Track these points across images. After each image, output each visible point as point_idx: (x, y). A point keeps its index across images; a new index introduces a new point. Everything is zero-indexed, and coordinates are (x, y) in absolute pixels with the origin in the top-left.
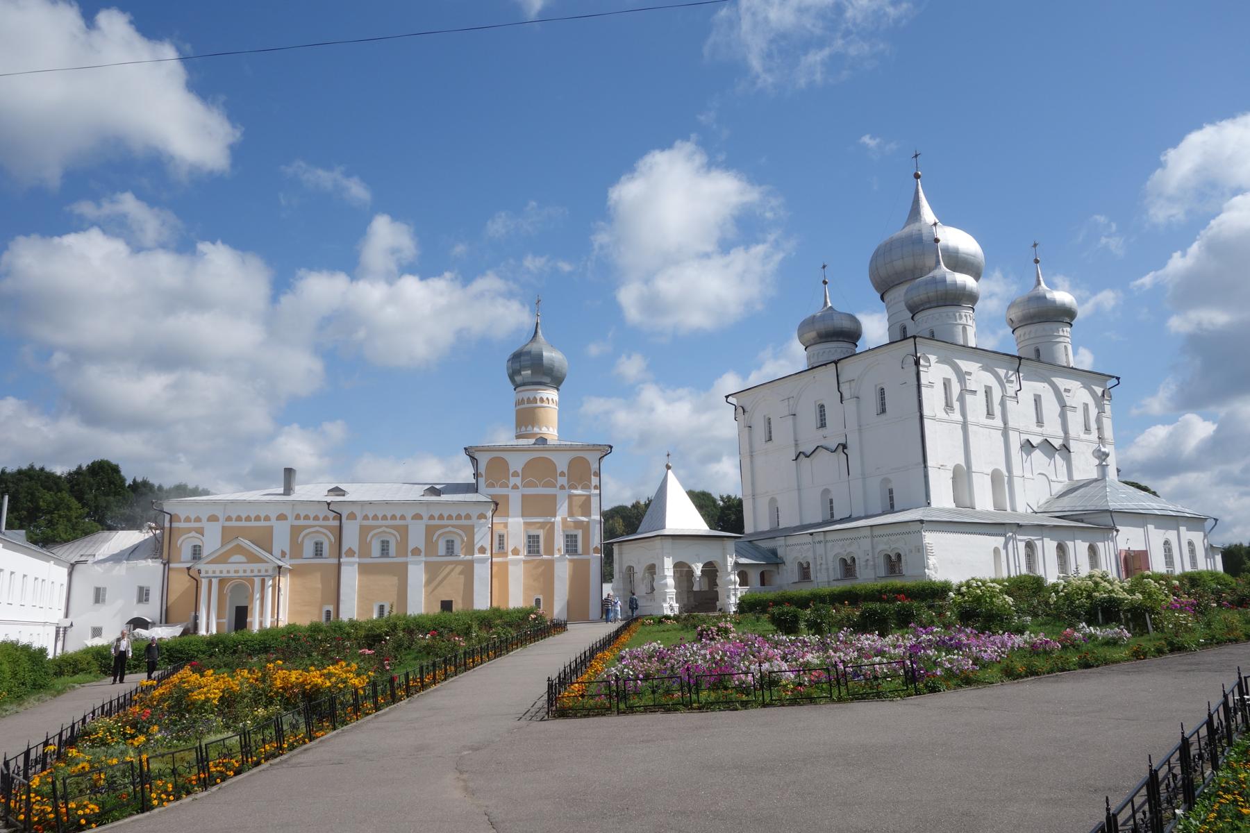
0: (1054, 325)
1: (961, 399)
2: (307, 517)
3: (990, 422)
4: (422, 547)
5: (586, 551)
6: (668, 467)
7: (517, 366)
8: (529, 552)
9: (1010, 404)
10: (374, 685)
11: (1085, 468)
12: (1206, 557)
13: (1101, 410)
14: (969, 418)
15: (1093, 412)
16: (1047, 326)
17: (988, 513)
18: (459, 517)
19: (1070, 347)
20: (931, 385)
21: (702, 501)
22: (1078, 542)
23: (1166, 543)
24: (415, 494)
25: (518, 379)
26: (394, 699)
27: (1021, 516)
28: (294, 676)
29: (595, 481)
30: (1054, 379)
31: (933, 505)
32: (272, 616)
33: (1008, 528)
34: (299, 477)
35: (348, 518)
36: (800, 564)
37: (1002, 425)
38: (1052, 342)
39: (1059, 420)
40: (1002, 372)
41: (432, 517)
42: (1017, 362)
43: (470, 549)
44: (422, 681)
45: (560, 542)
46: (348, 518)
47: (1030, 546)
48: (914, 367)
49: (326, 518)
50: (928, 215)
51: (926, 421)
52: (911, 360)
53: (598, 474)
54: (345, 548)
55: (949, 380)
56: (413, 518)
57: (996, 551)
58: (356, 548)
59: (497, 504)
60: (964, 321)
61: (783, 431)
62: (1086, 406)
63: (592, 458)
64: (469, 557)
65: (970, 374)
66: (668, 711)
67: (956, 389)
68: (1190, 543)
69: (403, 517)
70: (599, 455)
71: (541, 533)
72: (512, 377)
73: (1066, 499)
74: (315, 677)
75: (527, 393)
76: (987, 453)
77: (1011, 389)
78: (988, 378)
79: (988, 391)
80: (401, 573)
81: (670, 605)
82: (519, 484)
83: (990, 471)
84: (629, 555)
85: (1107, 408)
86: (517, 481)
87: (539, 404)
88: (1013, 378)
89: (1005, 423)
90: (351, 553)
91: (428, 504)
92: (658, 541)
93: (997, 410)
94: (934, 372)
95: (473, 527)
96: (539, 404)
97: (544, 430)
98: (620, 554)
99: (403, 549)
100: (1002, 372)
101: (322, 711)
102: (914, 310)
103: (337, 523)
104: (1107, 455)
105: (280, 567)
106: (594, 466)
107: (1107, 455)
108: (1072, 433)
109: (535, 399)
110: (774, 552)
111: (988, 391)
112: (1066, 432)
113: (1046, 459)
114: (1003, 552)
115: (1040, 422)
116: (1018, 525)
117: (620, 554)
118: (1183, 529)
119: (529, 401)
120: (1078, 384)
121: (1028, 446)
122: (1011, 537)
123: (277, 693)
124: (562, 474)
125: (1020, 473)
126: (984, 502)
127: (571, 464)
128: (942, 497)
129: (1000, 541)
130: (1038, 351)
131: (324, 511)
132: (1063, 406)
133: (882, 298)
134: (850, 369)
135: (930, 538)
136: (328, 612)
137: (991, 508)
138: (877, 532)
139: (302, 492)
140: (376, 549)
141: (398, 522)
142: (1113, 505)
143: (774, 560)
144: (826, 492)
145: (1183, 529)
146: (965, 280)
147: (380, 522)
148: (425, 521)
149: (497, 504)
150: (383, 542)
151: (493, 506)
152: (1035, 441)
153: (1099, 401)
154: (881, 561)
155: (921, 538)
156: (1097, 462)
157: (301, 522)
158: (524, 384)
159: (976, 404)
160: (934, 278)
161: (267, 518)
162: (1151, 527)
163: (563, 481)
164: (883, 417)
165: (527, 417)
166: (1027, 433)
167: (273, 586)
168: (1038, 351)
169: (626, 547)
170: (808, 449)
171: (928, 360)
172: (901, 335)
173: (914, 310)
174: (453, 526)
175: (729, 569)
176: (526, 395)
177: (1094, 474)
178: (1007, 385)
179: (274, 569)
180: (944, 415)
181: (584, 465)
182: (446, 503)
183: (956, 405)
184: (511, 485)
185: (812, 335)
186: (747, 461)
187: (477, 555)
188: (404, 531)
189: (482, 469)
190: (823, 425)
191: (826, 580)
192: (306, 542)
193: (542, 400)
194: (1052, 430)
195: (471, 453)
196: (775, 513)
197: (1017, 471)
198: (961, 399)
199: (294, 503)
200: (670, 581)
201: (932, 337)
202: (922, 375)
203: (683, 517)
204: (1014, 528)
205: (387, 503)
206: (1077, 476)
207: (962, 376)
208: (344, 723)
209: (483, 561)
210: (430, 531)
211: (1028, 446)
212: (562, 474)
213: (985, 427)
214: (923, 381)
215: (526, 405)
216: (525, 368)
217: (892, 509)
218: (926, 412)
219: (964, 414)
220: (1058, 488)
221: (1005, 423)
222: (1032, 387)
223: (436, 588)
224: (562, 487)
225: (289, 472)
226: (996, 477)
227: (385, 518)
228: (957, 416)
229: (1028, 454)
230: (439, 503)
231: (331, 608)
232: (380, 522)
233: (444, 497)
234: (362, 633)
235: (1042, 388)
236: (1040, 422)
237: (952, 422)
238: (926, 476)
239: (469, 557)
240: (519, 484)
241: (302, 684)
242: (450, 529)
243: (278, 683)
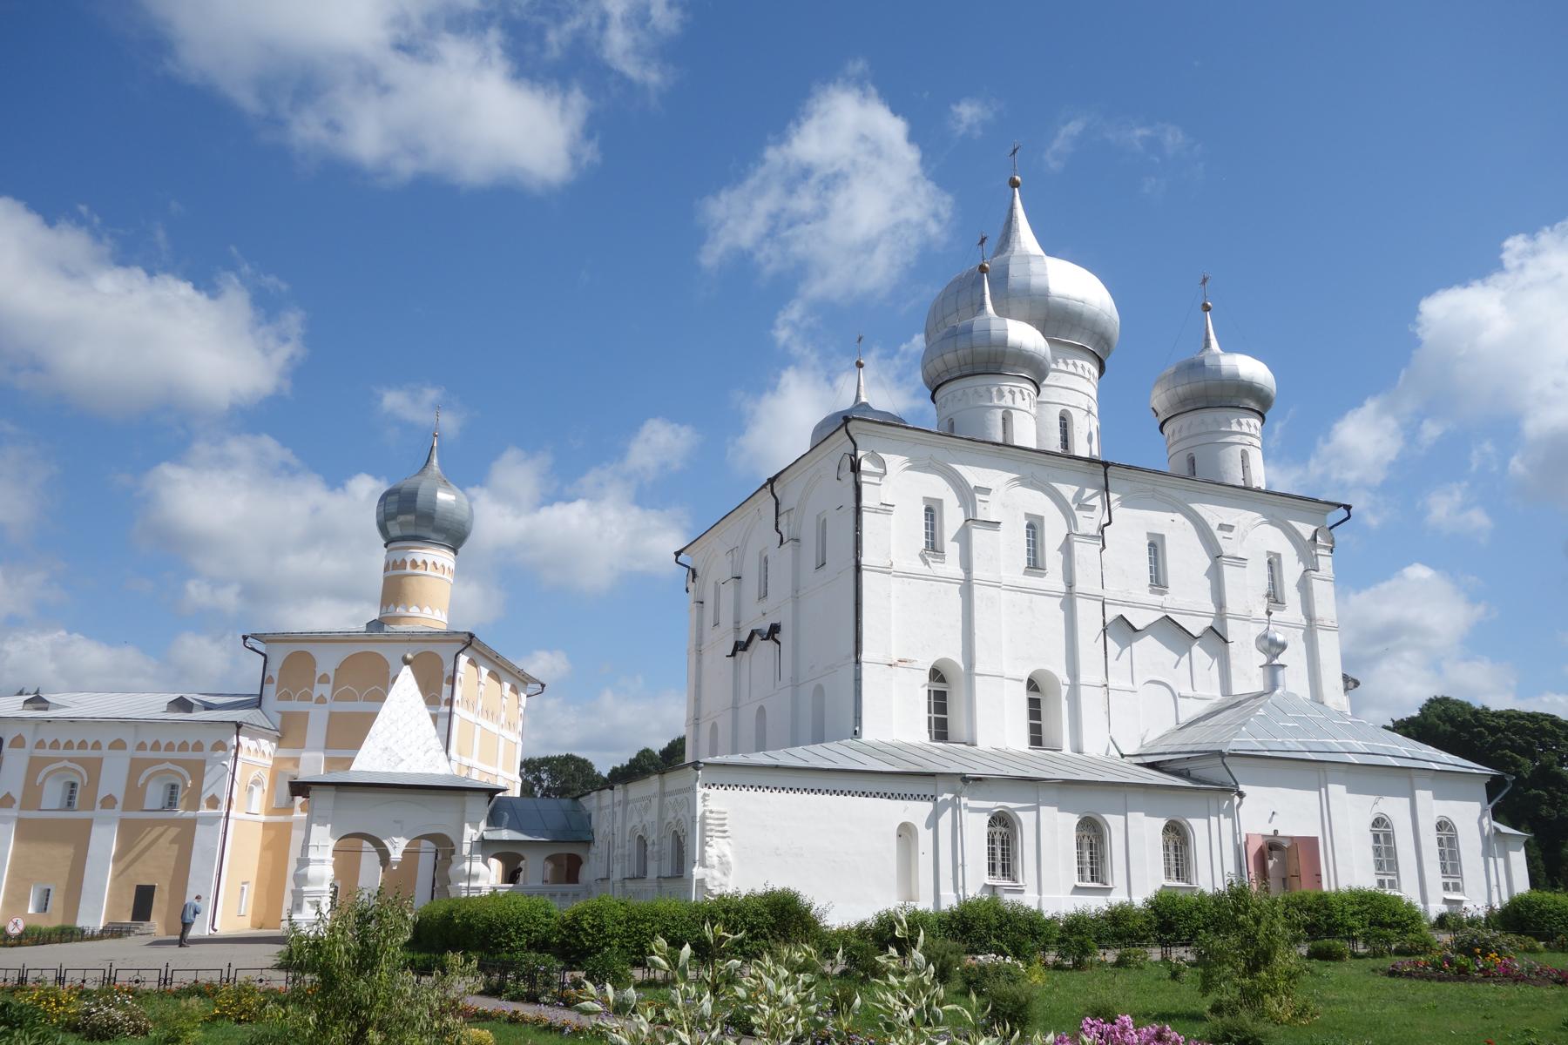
1: (964, 537)
3: (1033, 581)
4: (120, 796)
9: (1085, 552)
12: (1487, 853)
14: (976, 573)
15: (1292, 569)
16: (1208, 416)
18: (184, 746)
20: (886, 508)
23: (1379, 822)
27: (1093, 763)
29: (446, 688)
33: (941, 784)
35: (11, 746)
37: (1062, 588)
38: (1216, 442)
39: (1208, 583)
40: (1068, 491)
41: (142, 746)
46: (11, 746)
47: (1003, 824)
48: (849, 477)
50: (1026, 238)
51: (866, 576)
55: (1278, 556)
56: (112, 746)
57: (906, 832)
60: (1007, 401)
64: (190, 814)
65: (987, 491)
68: (1443, 825)
69: (97, 745)
72: (383, 528)
77: (1088, 523)
80: (79, 837)
82: (328, 696)
86: (324, 690)
88: (1097, 501)
89: (1070, 584)
95: (203, 763)
96: (409, 570)
104: (1283, 646)
106: (448, 668)
107: (1283, 646)
108: (1232, 606)
109: (404, 562)
112: (1220, 604)
114: (925, 837)
115: (1158, 581)
116: (965, 779)
121: (1122, 630)
122: (946, 803)
129: (917, 812)
132: (1217, 556)
141: (89, 753)
147: (61, 753)
152: (1140, 620)
153: (1307, 551)
156: (1263, 659)
159: (1000, 553)
162: (1337, 790)
166: (1125, 603)
174: (173, 761)
175: (466, 849)
176: (398, 556)
177: (1258, 685)
178: (1079, 514)
180: (918, 566)
183: (952, 549)
187: (204, 810)
188: (94, 767)
192: (48, 784)
193: (414, 564)
194: (1189, 598)
197: (1090, 672)
198: (964, 537)
202: (865, 489)
206: (1240, 687)
209: (213, 820)
211: (1122, 630)
218: (864, 561)
221: (1070, 584)
222: (1133, 525)
223: (127, 867)
228: (951, 566)
232: (61, 753)
235: (1174, 527)
236: (1158, 581)
238: (858, 680)
239: (190, 814)
240: (328, 696)
242: (168, 765)
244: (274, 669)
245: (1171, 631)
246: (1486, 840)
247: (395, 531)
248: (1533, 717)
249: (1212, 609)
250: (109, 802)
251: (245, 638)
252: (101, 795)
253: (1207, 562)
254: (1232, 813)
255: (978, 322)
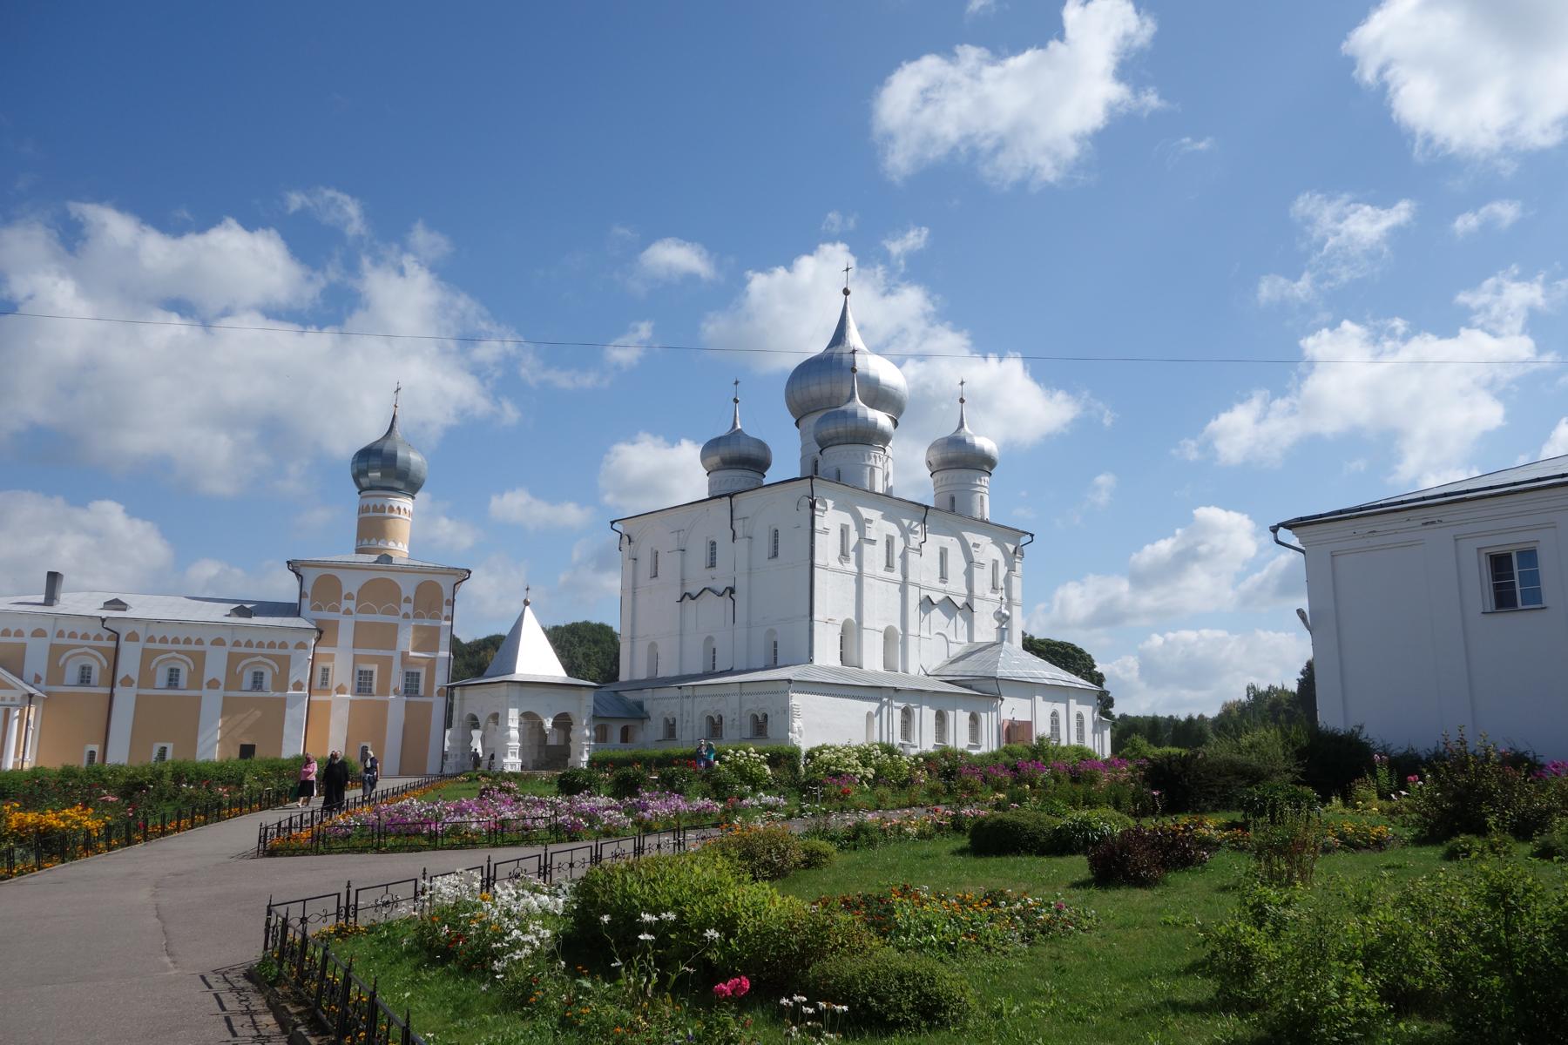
0: (973, 473)
1: (859, 549)
2: (73, 635)
3: (888, 575)
4: (222, 679)
5: (429, 692)
6: (526, 603)
7: (363, 466)
8: (359, 690)
10: (108, 828)
11: (986, 630)
12: (1094, 732)
13: (1011, 569)
14: (865, 570)
15: (1003, 571)
16: (965, 472)
17: (876, 674)
18: (272, 645)
19: (986, 498)
20: (826, 531)
21: (565, 640)
22: (960, 712)
23: (1054, 714)
24: (218, 613)
25: (364, 481)
26: (129, 842)
27: (915, 678)
28: (30, 818)
29: (446, 610)
30: (966, 534)
31: (816, 662)
32: (16, 755)
34: (66, 582)
36: (667, 720)
37: (900, 578)
40: (906, 522)
41: (237, 644)
42: (923, 512)
43: (281, 682)
44: (163, 827)
45: (397, 680)
47: (907, 713)
48: (809, 510)
49: (98, 638)
52: (808, 501)
53: (452, 603)
54: (120, 675)
57: (869, 715)
58: (135, 676)
59: (321, 632)
60: (872, 462)
61: (670, 565)
62: (995, 564)
63: (445, 583)
64: (277, 694)
65: (870, 521)
66: (360, 852)
67: (853, 537)
68: (1079, 716)
69: (199, 642)
70: (455, 579)
71: (375, 668)
72: (356, 478)
73: (961, 663)
74: (51, 819)
75: (374, 500)
76: (882, 608)
77: (915, 540)
78: (893, 529)
79: (890, 542)
81: (512, 762)
83: (883, 628)
84: (473, 700)
85: (1018, 566)
86: (351, 605)
87: (387, 514)
89: (905, 576)
90: (127, 682)
91: (234, 627)
92: (504, 687)
93: (897, 563)
94: (830, 519)
96: (387, 514)
97: (391, 545)
98: (462, 699)
99: (196, 680)
100: (906, 522)
101: (53, 847)
102: (824, 444)
103: (113, 644)
105: (31, 696)
106: (447, 595)
108: (977, 592)
109: (383, 507)
110: (640, 705)
111: (890, 542)
112: (971, 590)
113: (945, 620)
115: (943, 577)
116: (896, 690)
117: (462, 699)
118: (1073, 702)
119: (375, 509)
120: (989, 540)
121: (927, 604)
123: (11, 833)
124: (407, 600)
125: (916, 632)
126: (873, 661)
127: (421, 588)
128: (827, 654)
129: (873, 706)
130: (953, 499)
131: (95, 629)
132: (970, 562)
133: (797, 424)
134: (745, 503)
135: (797, 700)
136: (92, 754)
137: (881, 669)
138: (746, 689)
139: (68, 602)
140: (162, 677)
141: (193, 647)
142: (1001, 672)
143: (638, 713)
144: (709, 639)
145: (1073, 702)
146: (882, 419)
148: (228, 648)
149: (321, 632)
150: (171, 670)
151: (316, 634)
152: (936, 597)
154: (747, 721)
155: (787, 700)
156: (997, 624)
157: (65, 641)
158: (371, 488)
159: (874, 556)
160: (844, 412)
161: (19, 633)
162: (1039, 699)
163: (407, 608)
164: (774, 561)
165: (372, 528)
166: (929, 589)
167: (21, 718)
168: (953, 499)
169: (469, 692)
170: (694, 590)
171: (825, 505)
172: (812, 472)
173: (824, 444)
176: (372, 502)
177: (993, 638)
179: (23, 697)
180: (837, 565)
181: (436, 591)
182: (257, 627)
183: (852, 555)
184: (343, 609)
185: (715, 459)
186: (628, 597)
188: (199, 659)
189: (308, 589)
190: (713, 565)
191: (690, 738)
193: (391, 509)
194: (956, 587)
195: (294, 566)
196: (654, 659)
199: (58, 617)
200: (514, 734)
201: (838, 478)
203: (537, 660)
204: (892, 693)
205: (180, 623)
207: (862, 524)
208: (73, 858)
210: (233, 660)
211: (927, 604)
212: (407, 600)
213: (883, 579)
214: (818, 526)
215: (371, 514)
216: (374, 469)
217: (774, 665)
218: (818, 560)
219: (859, 565)
220: (956, 650)
221: (905, 576)
222: (934, 542)
224: (406, 616)
225: (54, 578)
226: (889, 635)
227: (176, 641)
228: (852, 566)
229: (927, 612)
230: (247, 627)
231: (96, 748)
233: (256, 620)
234: (122, 780)
236: (943, 577)
237: (846, 572)
241: (37, 826)
243: (14, 824)
244: (308, 589)
245: (948, 606)
246: (1095, 724)
247: (364, 481)
248: (1061, 644)
249: (966, 592)
250: (214, 684)
251: (1274, 530)
252: (206, 679)
253: (965, 566)
254: (996, 709)
255: (849, 407)
